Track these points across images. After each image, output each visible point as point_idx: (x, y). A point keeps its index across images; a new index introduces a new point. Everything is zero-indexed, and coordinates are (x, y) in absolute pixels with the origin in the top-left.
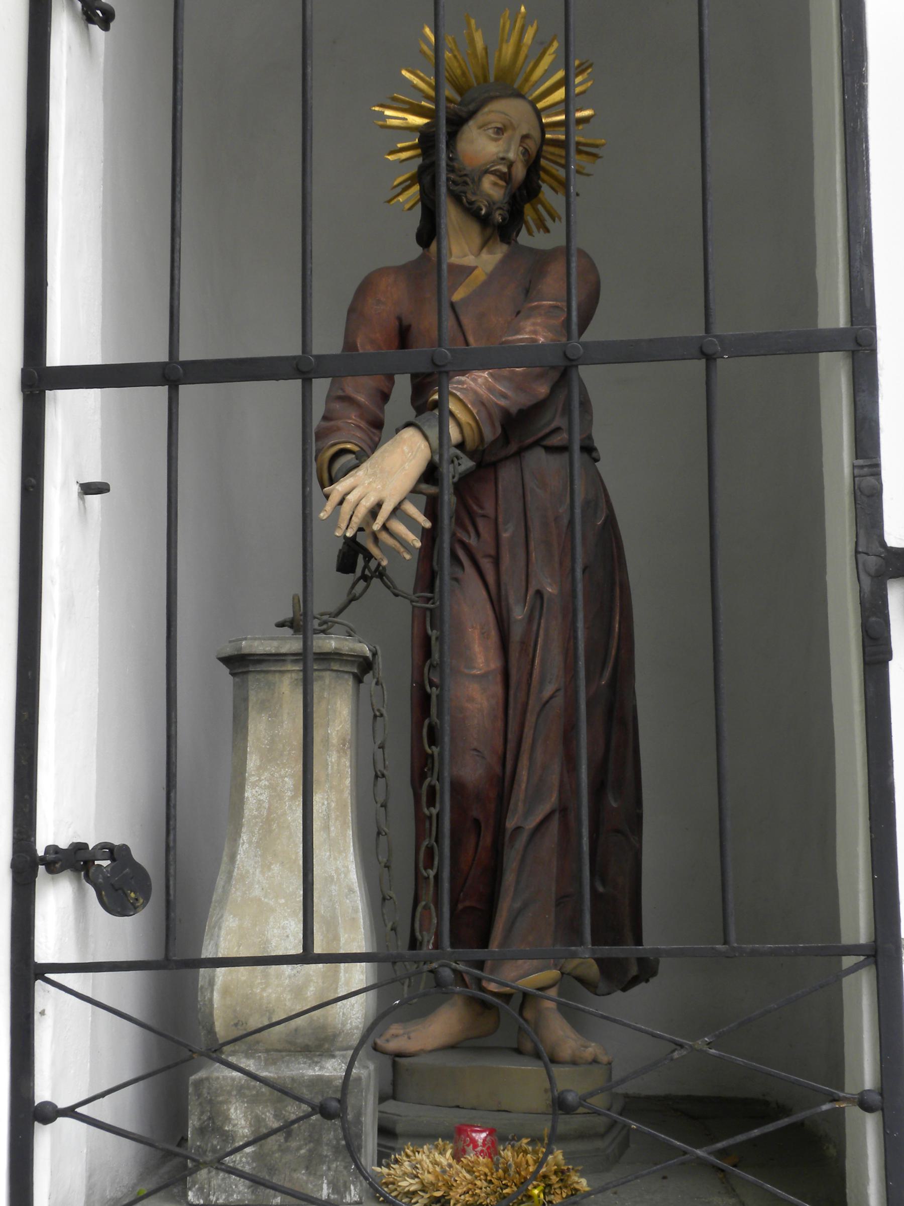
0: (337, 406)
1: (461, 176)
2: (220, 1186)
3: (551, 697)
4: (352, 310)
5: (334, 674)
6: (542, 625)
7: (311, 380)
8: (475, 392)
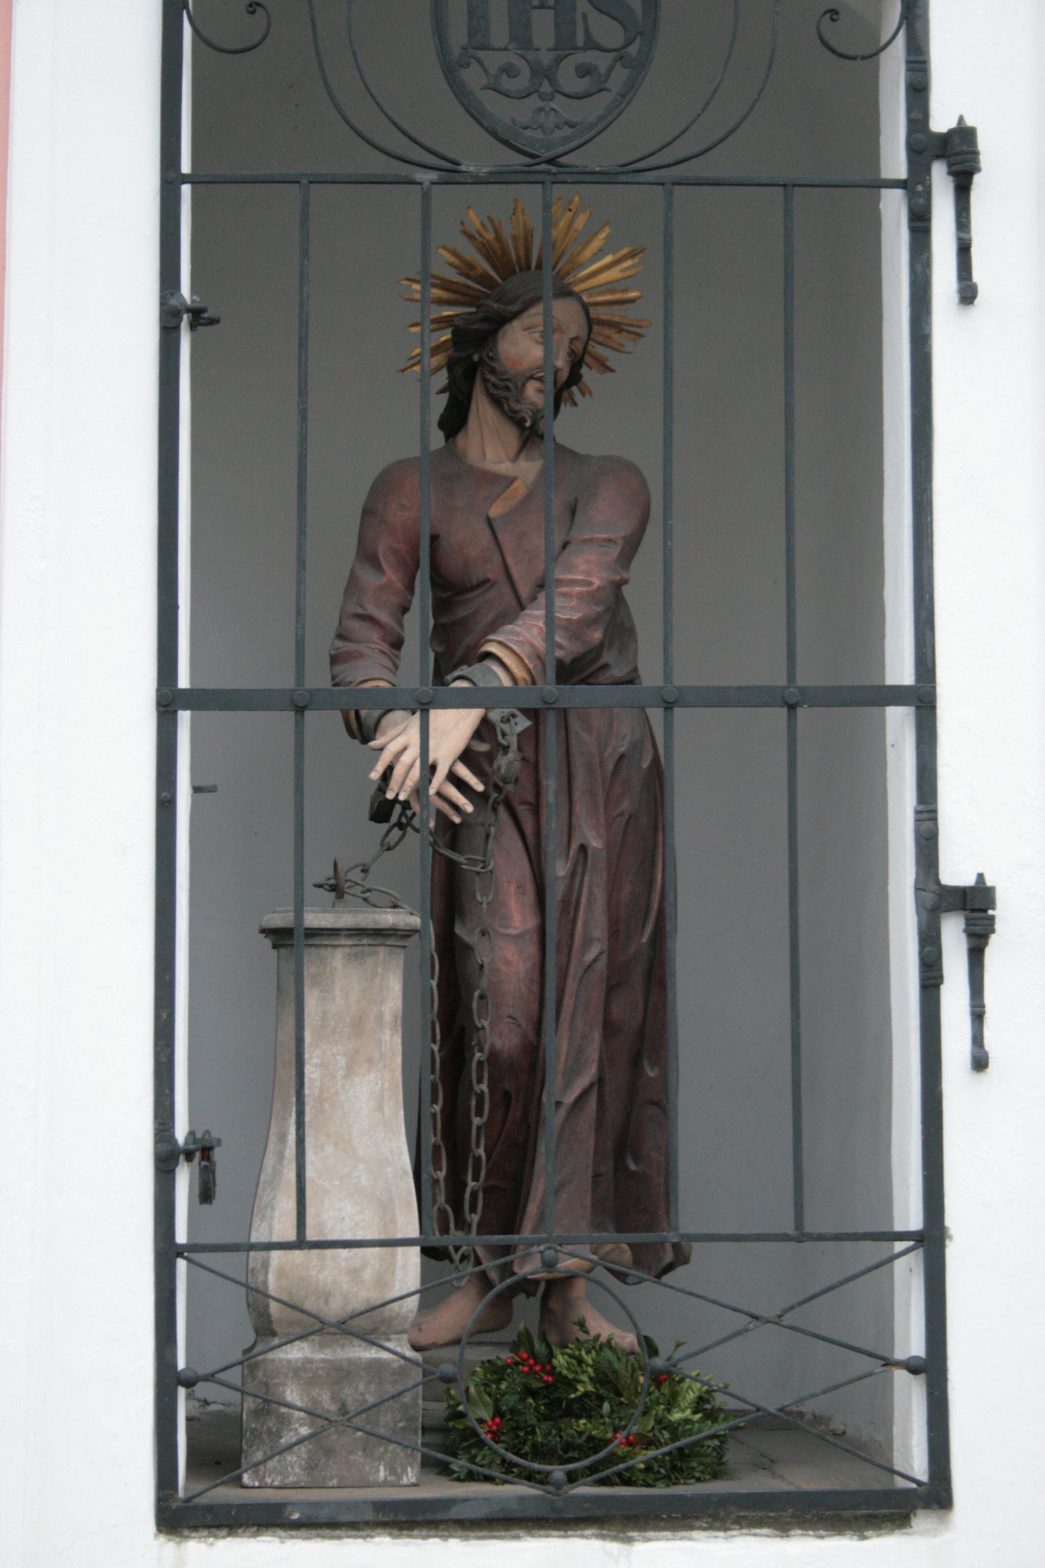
0: (356, 625)
1: (502, 380)
2: (275, 1468)
3: (595, 961)
4: (367, 512)
5: (388, 949)
6: (586, 883)
7: (428, 711)
8: (532, 645)
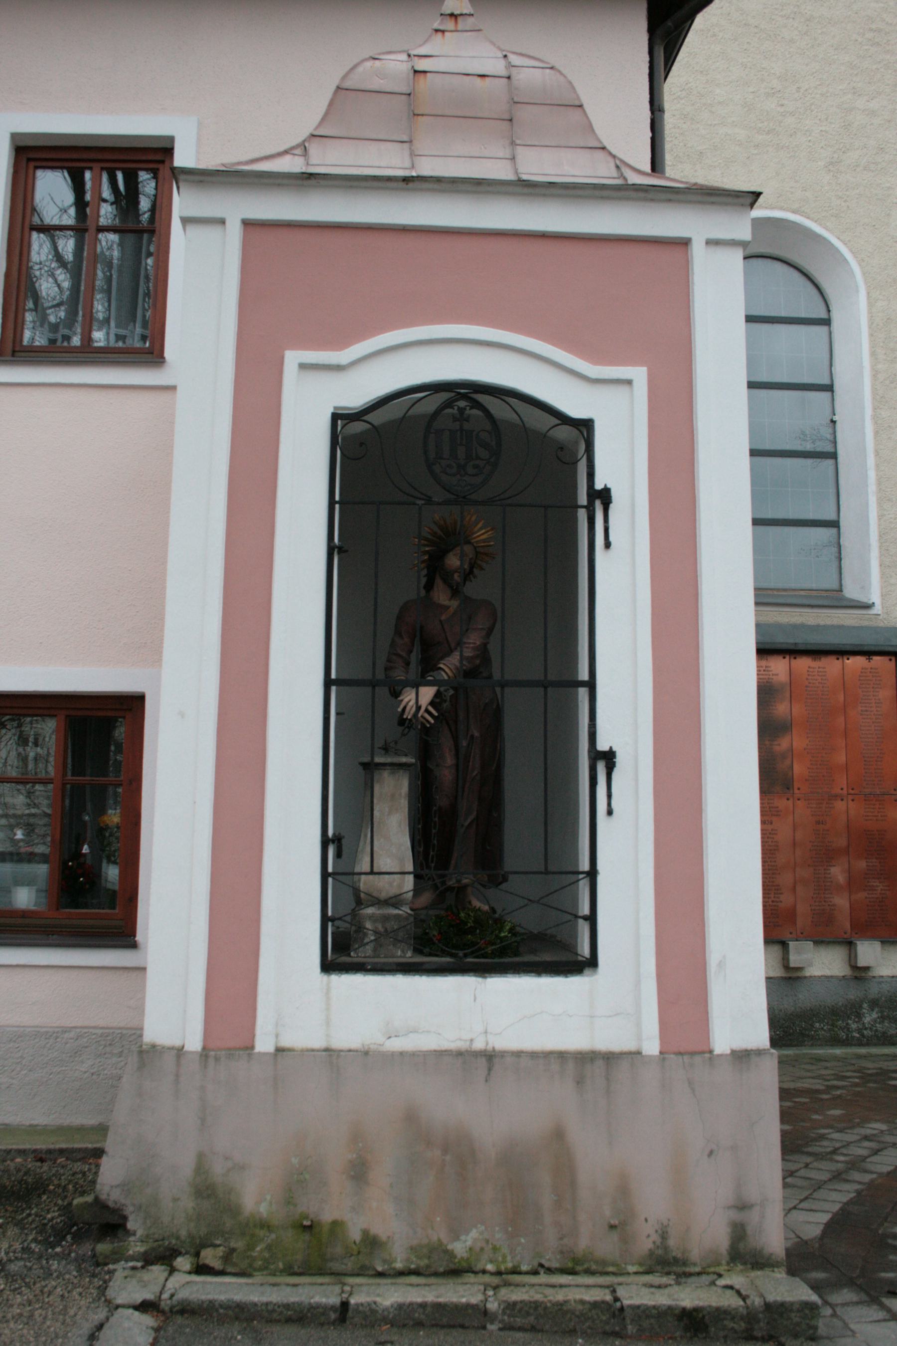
0: (394, 657)
